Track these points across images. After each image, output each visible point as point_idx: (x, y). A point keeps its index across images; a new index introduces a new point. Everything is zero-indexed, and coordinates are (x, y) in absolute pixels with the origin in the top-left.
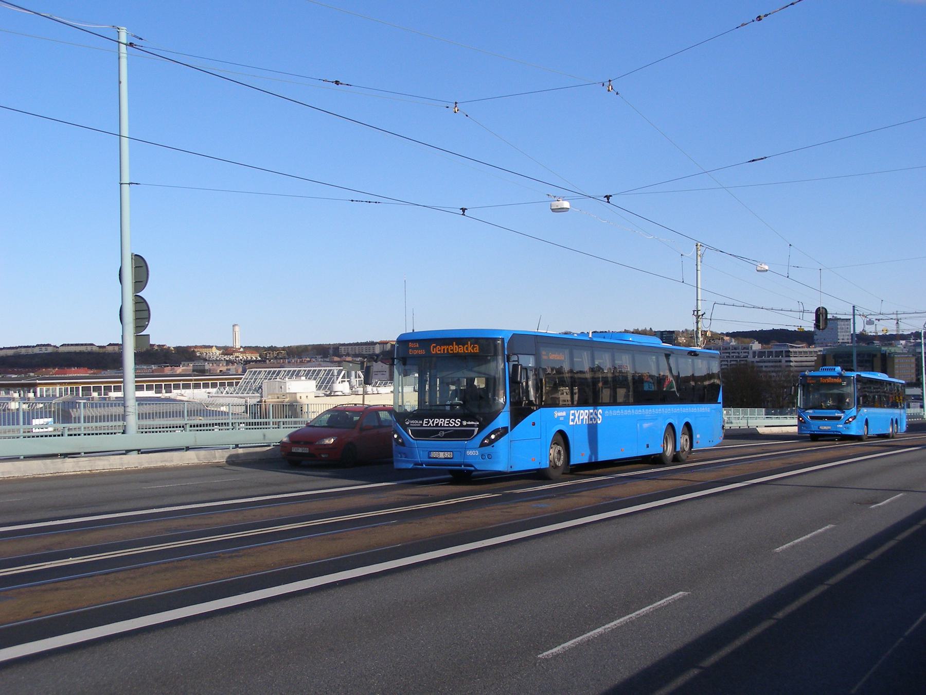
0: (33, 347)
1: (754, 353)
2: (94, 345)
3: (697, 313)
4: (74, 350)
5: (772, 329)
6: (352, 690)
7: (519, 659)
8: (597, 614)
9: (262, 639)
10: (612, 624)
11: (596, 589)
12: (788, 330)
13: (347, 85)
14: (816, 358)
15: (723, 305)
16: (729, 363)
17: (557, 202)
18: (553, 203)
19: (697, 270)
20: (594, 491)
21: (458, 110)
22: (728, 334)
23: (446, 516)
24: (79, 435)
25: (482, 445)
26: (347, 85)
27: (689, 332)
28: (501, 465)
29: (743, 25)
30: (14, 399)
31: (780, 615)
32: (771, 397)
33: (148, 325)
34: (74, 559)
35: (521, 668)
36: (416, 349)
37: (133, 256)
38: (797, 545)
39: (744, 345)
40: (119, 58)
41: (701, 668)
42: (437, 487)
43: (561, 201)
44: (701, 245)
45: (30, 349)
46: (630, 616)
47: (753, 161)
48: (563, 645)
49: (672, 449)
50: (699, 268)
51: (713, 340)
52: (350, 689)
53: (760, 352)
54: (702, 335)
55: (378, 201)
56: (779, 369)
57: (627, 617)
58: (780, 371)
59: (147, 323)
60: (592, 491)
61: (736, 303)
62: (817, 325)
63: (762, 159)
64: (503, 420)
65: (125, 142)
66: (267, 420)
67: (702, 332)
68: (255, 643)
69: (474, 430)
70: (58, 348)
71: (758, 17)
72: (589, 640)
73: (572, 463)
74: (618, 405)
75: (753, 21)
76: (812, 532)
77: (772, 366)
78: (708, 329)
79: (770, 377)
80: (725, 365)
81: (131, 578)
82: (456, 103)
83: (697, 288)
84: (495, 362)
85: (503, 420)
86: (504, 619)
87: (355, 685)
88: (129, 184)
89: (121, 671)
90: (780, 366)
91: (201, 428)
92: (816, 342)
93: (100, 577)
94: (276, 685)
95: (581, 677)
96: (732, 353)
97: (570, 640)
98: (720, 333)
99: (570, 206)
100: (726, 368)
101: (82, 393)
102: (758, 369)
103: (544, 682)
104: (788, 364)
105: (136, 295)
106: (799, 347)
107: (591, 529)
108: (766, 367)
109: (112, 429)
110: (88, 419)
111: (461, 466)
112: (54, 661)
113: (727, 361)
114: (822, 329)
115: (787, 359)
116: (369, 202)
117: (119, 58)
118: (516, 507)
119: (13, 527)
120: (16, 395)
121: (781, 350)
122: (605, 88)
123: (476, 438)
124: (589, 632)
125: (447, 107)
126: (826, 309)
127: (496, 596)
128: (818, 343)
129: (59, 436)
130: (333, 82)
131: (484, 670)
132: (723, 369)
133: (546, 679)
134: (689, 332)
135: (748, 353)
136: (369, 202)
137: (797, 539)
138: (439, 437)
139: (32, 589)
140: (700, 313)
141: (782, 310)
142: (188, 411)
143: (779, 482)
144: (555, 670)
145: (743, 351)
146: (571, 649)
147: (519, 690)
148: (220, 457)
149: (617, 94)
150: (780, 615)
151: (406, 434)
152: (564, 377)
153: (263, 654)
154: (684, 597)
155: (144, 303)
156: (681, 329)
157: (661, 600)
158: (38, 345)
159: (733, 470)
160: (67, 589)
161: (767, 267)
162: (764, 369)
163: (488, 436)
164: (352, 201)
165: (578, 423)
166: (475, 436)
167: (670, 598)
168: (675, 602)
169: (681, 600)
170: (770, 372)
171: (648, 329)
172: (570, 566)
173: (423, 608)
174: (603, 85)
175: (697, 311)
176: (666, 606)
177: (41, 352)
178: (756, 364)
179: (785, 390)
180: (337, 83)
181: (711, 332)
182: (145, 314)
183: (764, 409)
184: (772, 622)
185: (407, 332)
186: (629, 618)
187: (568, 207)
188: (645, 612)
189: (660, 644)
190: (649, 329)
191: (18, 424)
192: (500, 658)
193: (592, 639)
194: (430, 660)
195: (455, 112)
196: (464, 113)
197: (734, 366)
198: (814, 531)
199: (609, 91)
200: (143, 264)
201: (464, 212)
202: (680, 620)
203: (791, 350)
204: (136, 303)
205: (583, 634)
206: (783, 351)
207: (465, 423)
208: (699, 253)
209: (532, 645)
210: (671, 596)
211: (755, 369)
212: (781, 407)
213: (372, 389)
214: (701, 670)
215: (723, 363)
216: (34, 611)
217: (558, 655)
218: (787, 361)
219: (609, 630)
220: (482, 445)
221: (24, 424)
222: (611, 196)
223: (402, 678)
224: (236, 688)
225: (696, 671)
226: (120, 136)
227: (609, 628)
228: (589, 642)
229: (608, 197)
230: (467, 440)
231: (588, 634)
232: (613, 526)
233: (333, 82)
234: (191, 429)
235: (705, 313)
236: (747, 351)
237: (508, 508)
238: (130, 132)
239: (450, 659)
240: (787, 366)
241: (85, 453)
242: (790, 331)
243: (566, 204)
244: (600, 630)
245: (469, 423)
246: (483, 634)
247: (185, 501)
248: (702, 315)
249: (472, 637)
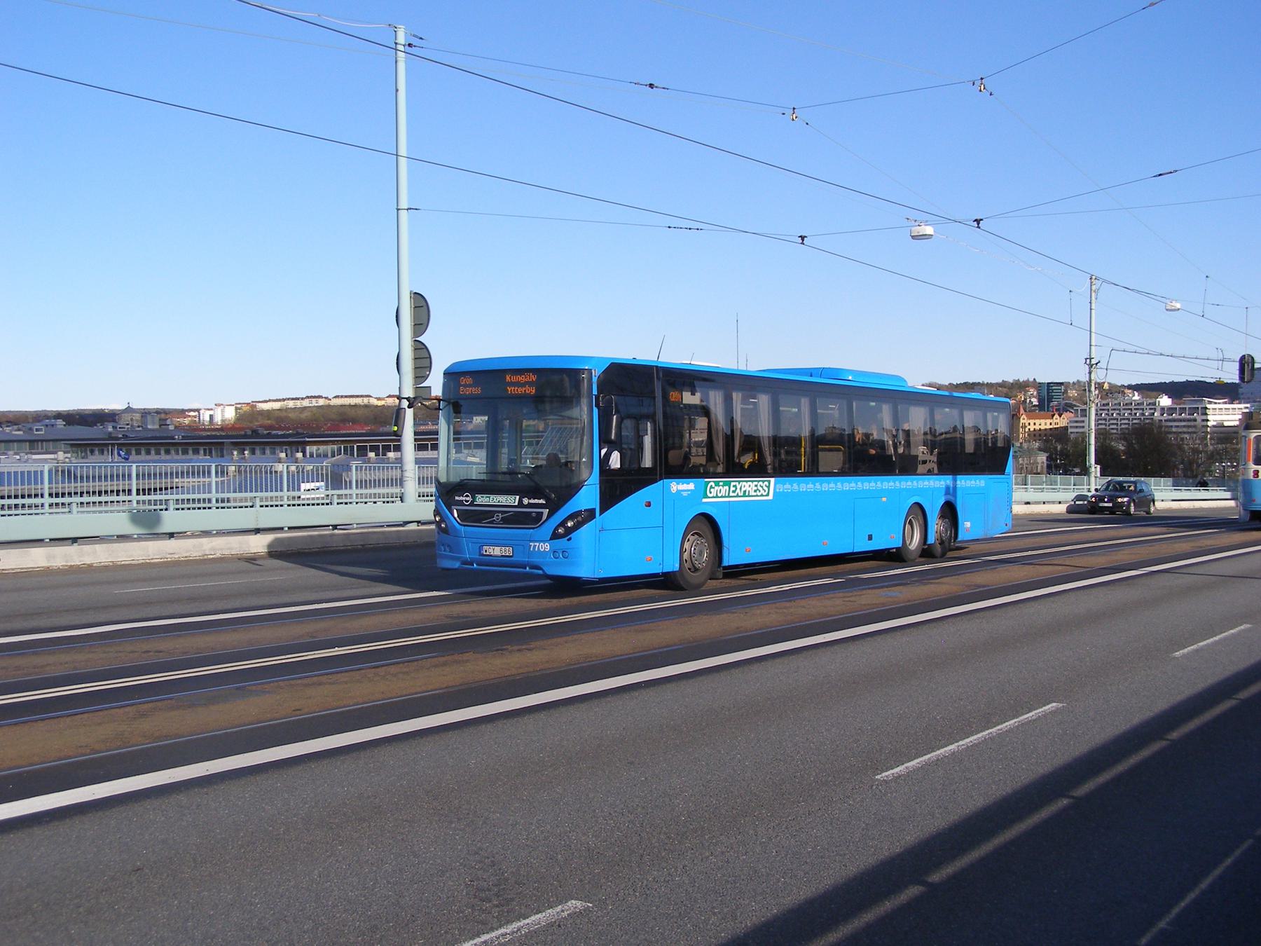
0: (302, 399)
1: (1163, 409)
2: (371, 397)
3: (1090, 361)
4: (354, 402)
5: (1185, 380)
7: (853, 780)
8: (950, 727)
9: (550, 748)
10: (967, 740)
11: (952, 697)
13: (664, 88)
14: (1240, 417)
15: (1123, 352)
17: (918, 227)
18: (913, 229)
19: (1091, 309)
20: (957, 577)
21: (796, 117)
22: (1130, 387)
23: (778, 605)
24: (281, 506)
25: (555, 536)
26: (664, 88)
27: (1082, 384)
28: (585, 569)
31: (1175, 735)
33: (429, 375)
36: (470, 386)
37: (412, 295)
38: (1202, 649)
41: (1073, 797)
42: (509, 600)
44: (1096, 279)
45: (299, 401)
46: (990, 731)
47: (1160, 175)
48: (906, 765)
49: (920, 540)
50: (1093, 307)
52: (650, 810)
53: (1170, 408)
54: (1096, 388)
56: (1193, 430)
57: (987, 732)
58: (1195, 433)
59: (428, 373)
60: (954, 577)
61: (1139, 350)
62: (1242, 378)
63: (1171, 173)
64: (588, 497)
65: (403, 161)
66: (206, 496)
68: (542, 753)
69: (542, 513)
70: (330, 400)
73: (726, 563)
74: (821, 476)
77: (1184, 426)
78: (1104, 381)
79: (1182, 439)
80: (1125, 424)
81: (404, 673)
82: (794, 109)
83: (1091, 331)
84: (579, 408)
85: (588, 497)
86: (838, 731)
87: (657, 806)
88: (407, 210)
89: (388, 781)
90: (1195, 426)
91: (223, 505)
92: (1242, 396)
93: (368, 670)
94: (564, 803)
95: (926, 804)
96: (1100, 410)
97: (915, 759)
98: (1120, 385)
100: (1126, 429)
101: (357, 454)
102: (1166, 429)
103: (882, 808)
104: (1205, 423)
105: (415, 340)
106: (1219, 403)
107: (951, 624)
109: (276, 501)
110: (361, 484)
111: (526, 568)
113: (1129, 419)
114: (1247, 382)
115: (1204, 417)
116: (690, 229)
117: (396, 62)
118: (861, 595)
119: (36, 635)
120: (283, 455)
121: (1197, 406)
122: (977, 87)
123: (546, 524)
124: (939, 749)
125: (784, 114)
126: (1253, 358)
127: (831, 703)
128: (1243, 398)
129: (327, 504)
130: (646, 85)
131: (810, 792)
133: (883, 804)
134: (1082, 384)
135: (1155, 409)
136: (690, 229)
137: (1202, 641)
138: (187, 536)
139: (292, 682)
140: (1093, 362)
142: (357, 481)
143: (1184, 571)
144: (894, 794)
145: (1148, 407)
146: (916, 770)
147: (850, 817)
148: (258, 544)
149: (991, 94)
150: (1175, 735)
151: (449, 515)
153: (550, 766)
154: (1058, 709)
155: (425, 350)
157: (1028, 713)
158: (308, 397)
160: (330, 684)
161: (1178, 306)
162: (1174, 430)
163: (563, 524)
164: (669, 227)
166: (544, 522)
168: (1045, 715)
170: (1180, 433)
171: (1031, 380)
172: (921, 669)
173: (742, 715)
174: (974, 84)
175: (1091, 359)
176: (1034, 720)
177: (311, 405)
178: (1164, 423)
180: (651, 86)
181: (1108, 383)
182: (426, 363)
184: (1164, 743)
186: (989, 734)
187: (932, 233)
189: (1024, 766)
190: (1032, 380)
191: (281, 490)
192: (830, 778)
194: (746, 778)
195: (793, 120)
196: (804, 121)
199: (981, 91)
201: (803, 240)
202: (1050, 738)
203: (1208, 406)
207: (526, 501)
208: (1094, 287)
209: (869, 763)
210: (1042, 707)
211: (1163, 429)
213: (697, 450)
214: (1072, 800)
216: (293, 709)
217: (900, 777)
218: (1203, 420)
219: (963, 747)
220: (555, 536)
222: (982, 220)
223: (712, 799)
224: (518, 805)
225: (1065, 801)
226: (397, 155)
227: (963, 745)
228: (938, 761)
229: (978, 221)
230: (533, 528)
231: (938, 752)
232: (977, 620)
233: (646, 85)
234: (420, 498)
235: (1099, 362)
238: (408, 149)
239: (770, 778)
241: (289, 528)
243: (929, 230)
245: (532, 501)
246: (811, 748)
247: (91, 620)
248: (1096, 364)
249: (798, 752)
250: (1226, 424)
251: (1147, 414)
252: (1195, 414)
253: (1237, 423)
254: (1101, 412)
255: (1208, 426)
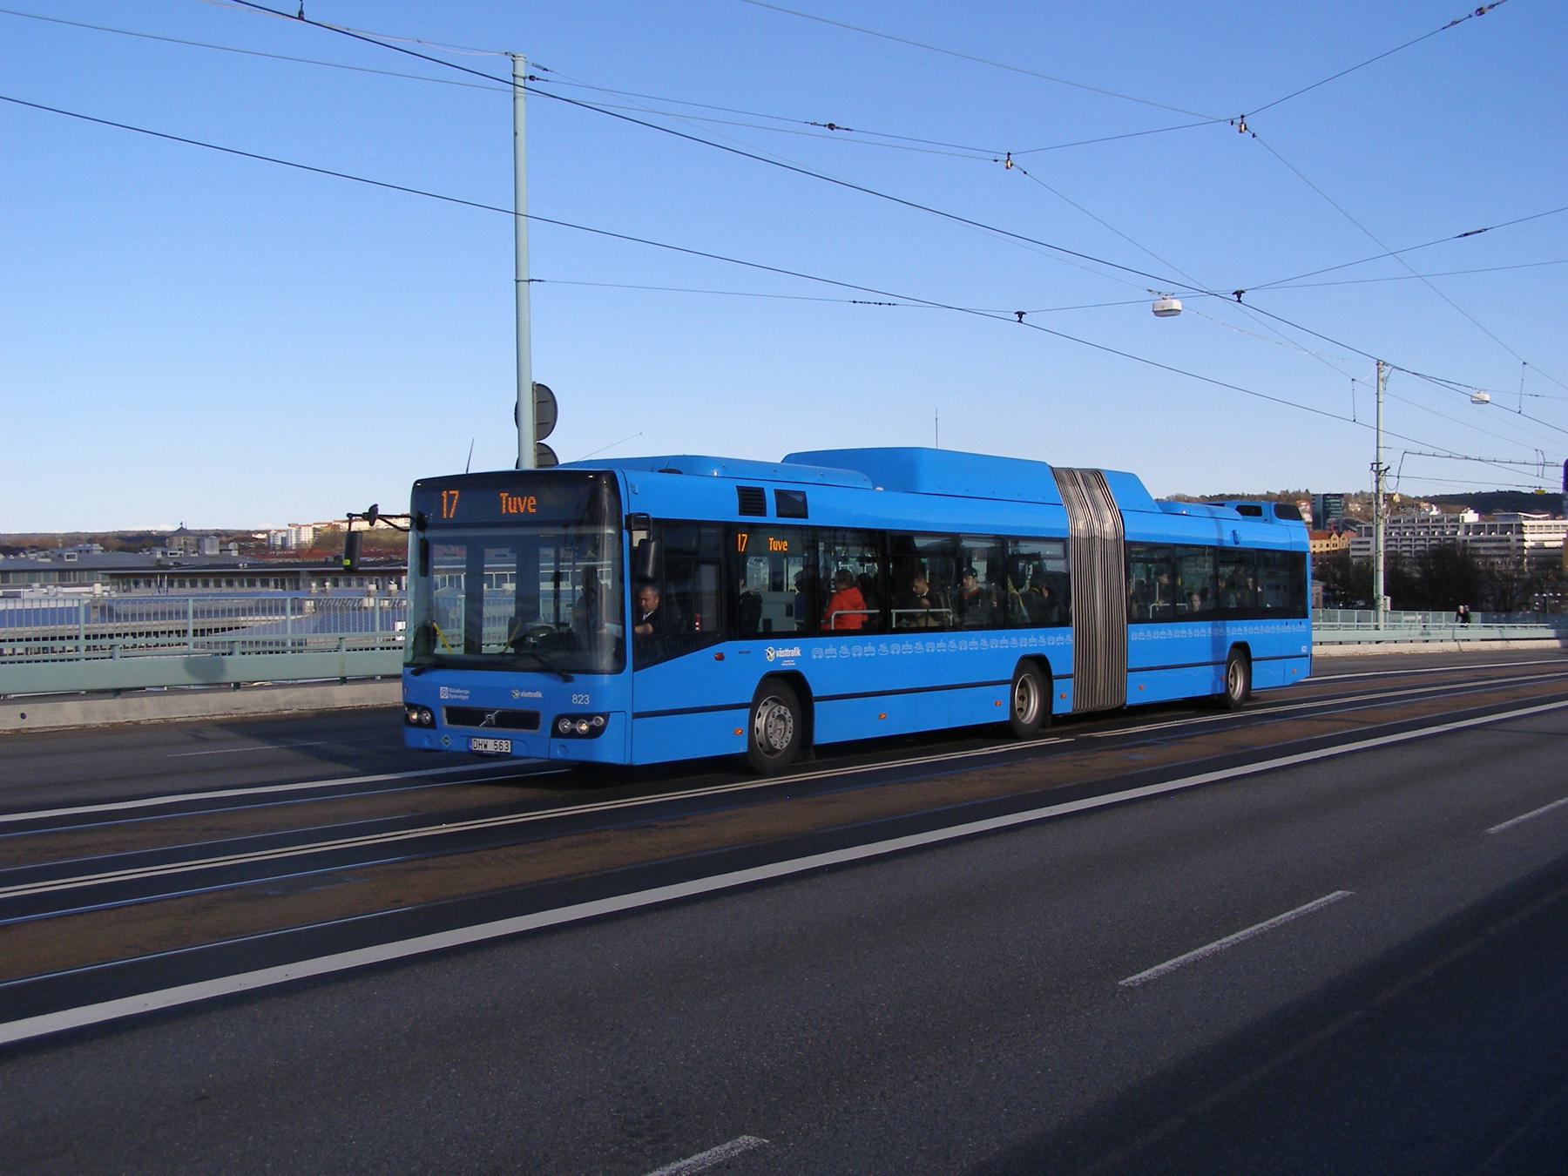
1: (1468, 526)
3: (1378, 467)
5: (1495, 491)
6: (841, 1026)
10: (1232, 937)
12: (1521, 493)
14: (1565, 536)
16: (1413, 543)
17: (1163, 301)
19: (1378, 402)
21: (1011, 165)
22: (1427, 499)
26: (847, 129)
27: (1367, 496)
29: (1454, 23)
30: (369, 594)
32: (1493, 594)
34: (449, 826)
35: (1093, 1000)
38: (1523, 823)
39: (1452, 516)
40: (514, 99)
43: (1169, 300)
46: (1261, 925)
47: (1466, 235)
51: (1403, 507)
54: (1384, 500)
55: (892, 303)
56: (1507, 552)
57: (1257, 927)
61: (1438, 452)
67: (1384, 496)
71: (1478, 10)
72: (1196, 961)
75: (1470, 16)
76: (1547, 803)
77: (1495, 548)
78: (1394, 492)
90: (1508, 548)
96: (1432, 527)
98: (1413, 496)
99: (1183, 306)
100: (1423, 551)
102: (1472, 552)
104: (1520, 544)
106: (1538, 519)
108: (1485, 548)
112: (418, 971)
113: (1425, 540)
115: (1519, 537)
116: (880, 304)
122: (1236, 127)
124: (1196, 948)
132: (1418, 551)
134: (1367, 496)
136: (880, 304)
140: (1382, 467)
141: (1510, 462)
145: (1449, 525)
146: (1170, 974)
149: (1254, 136)
152: (603, 561)
156: (1352, 490)
159: (1428, 706)
161: (1487, 397)
164: (854, 302)
165: (519, 499)
167: (1323, 899)
169: (1339, 903)
171: (1303, 491)
175: (1378, 464)
179: (1515, 585)
180: (831, 126)
181: (1400, 495)
183: (1480, 613)
185: (469, 472)
188: (1283, 920)
193: (1201, 959)
197: (1435, 547)
198: (1551, 803)
199: (1241, 131)
200: (550, 398)
203: (1525, 523)
204: (539, 454)
205: (1188, 952)
206: (1512, 525)
211: (1468, 552)
212: (1508, 611)
215: (1390, 543)
218: (1519, 540)
221: (194, 636)
226: (516, 214)
229: (1239, 294)
231: (1196, 952)
235: (1389, 468)
236: (1456, 524)
237: (1085, 759)
240: (1518, 548)
242: (1525, 494)
243: (1176, 305)
244: (1214, 945)
248: (1385, 470)
250: (1547, 544)
251: (1447, 533)
252: (1508, 533)
253: (1561, 543)
254: (1434, 530)
255: (1525, 548)
